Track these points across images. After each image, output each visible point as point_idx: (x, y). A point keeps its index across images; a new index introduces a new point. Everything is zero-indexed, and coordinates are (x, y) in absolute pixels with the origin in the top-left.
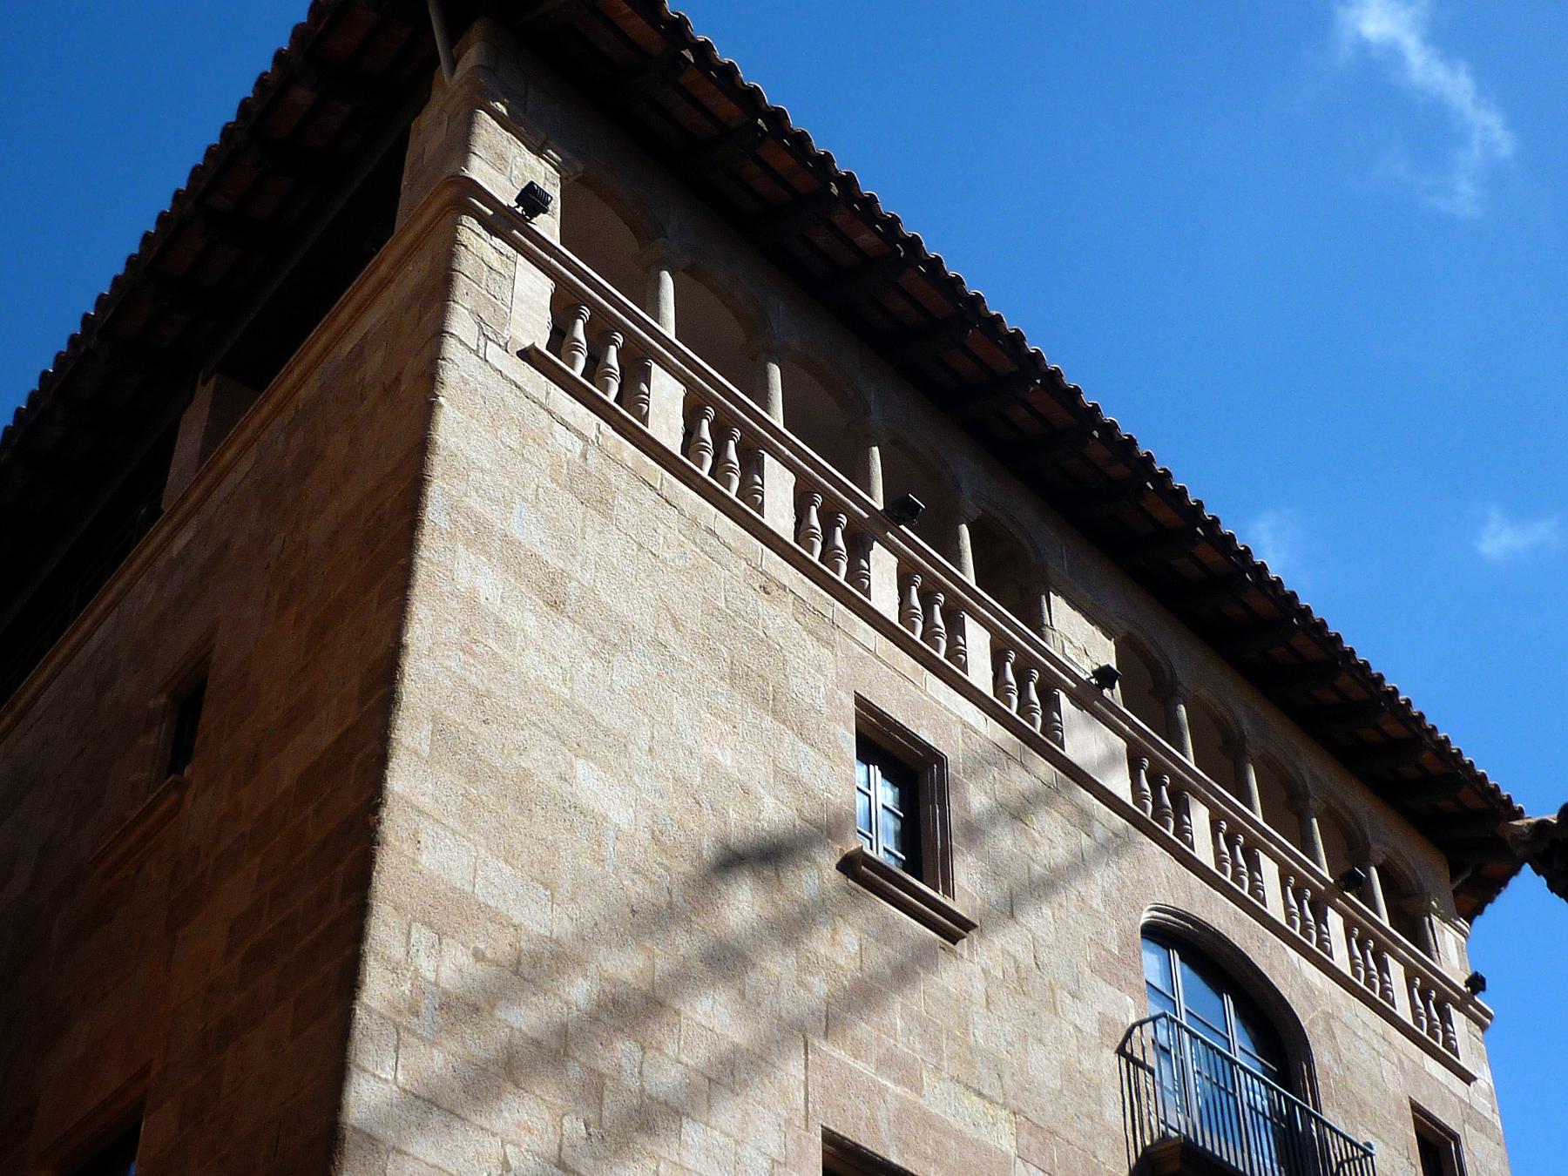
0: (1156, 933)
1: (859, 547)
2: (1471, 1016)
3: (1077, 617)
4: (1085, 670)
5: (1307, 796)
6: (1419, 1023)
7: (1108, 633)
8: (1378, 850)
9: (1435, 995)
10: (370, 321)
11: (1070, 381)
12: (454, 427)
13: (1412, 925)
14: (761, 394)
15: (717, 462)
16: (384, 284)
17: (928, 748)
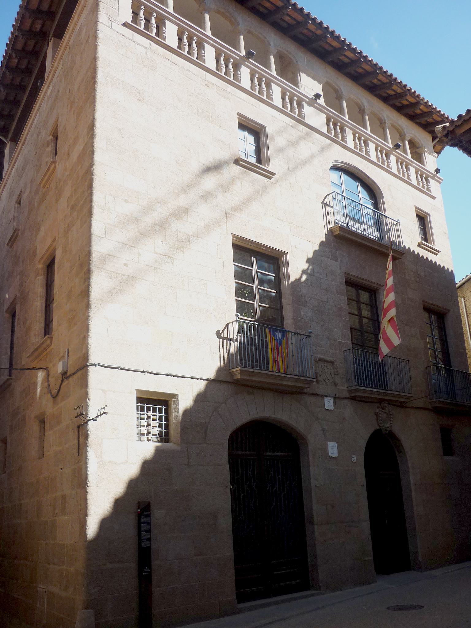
0: (334, 168)
1: (236, 67)
2: (436, 180)
3: (310, 79)
4: (311, 95)
5: (385, 122)
6: (419, 185)
7: (320, 82)
8: (408, 137)
9: (424, 177)
10: (82, 19)
11: (300, 6)
12: (104, 52)
13: (418, 157)
14: (201, 24)
15: (189, 47)
16: (84, 7)
17: (261, 125)
